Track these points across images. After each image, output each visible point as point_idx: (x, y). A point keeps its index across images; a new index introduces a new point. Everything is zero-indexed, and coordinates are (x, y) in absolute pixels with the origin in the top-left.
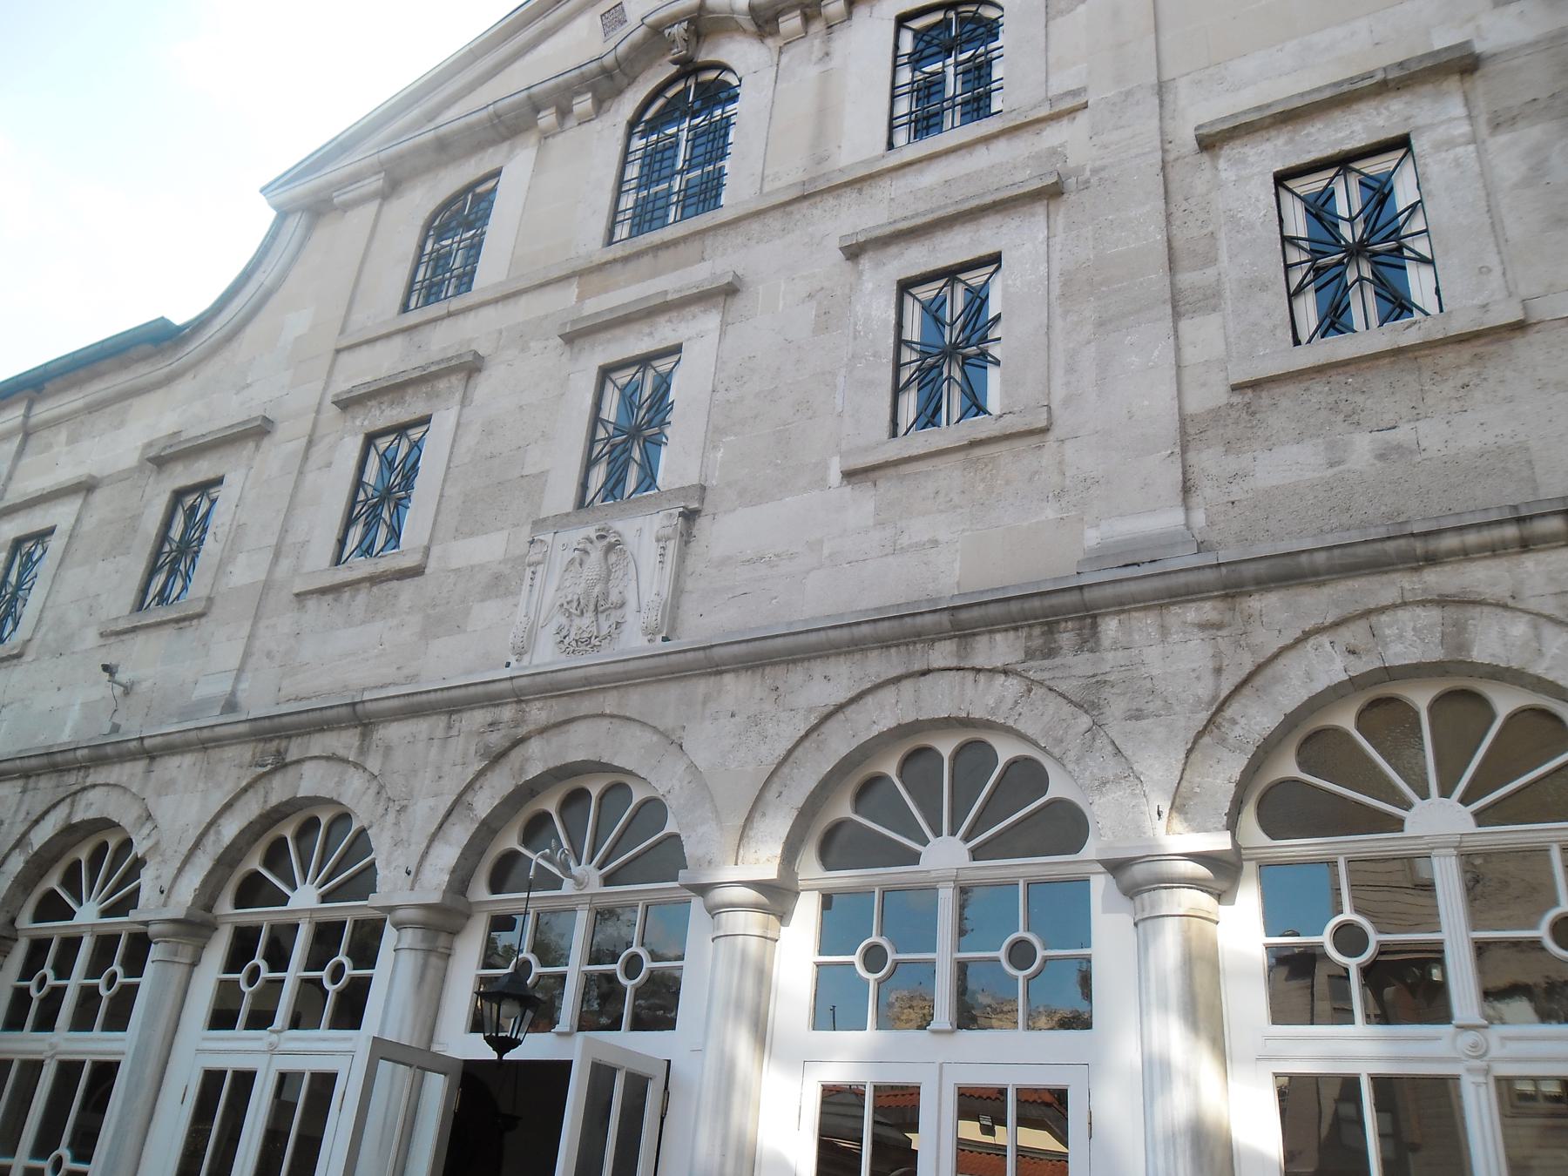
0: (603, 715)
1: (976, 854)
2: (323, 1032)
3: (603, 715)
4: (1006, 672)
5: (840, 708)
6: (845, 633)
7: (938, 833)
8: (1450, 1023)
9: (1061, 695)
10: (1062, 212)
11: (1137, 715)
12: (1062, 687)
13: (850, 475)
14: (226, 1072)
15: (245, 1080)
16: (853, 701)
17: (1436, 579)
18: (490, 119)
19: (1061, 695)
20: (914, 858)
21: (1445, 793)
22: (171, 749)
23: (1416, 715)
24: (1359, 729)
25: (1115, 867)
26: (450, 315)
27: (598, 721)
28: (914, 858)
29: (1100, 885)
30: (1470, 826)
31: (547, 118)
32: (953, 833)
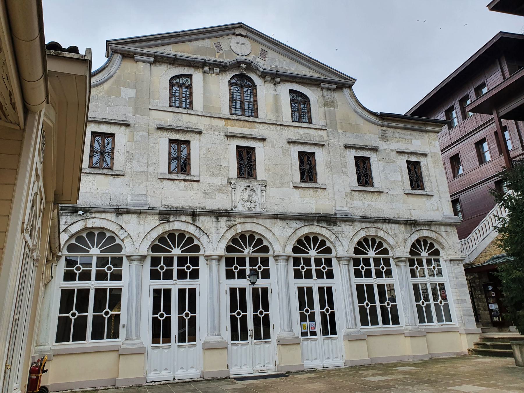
0: (254, 223)
1: (318, 253)
2: (161, 280)
3: (254, 223)
4: (324, 227)
5: (299, 228)
6: (268, 215)
7: (175, 248)
8: (312, 278)
9: (332, 232)
10: (128, 129)
11: (342, 237)
12: (332, 231)
13: (294, 187)
14: (88, 290)
15: (168, 292)
16: (301, 227)
17: (376, 225)
18: (192, 61)
19: (332, 232)
20: (171, 252)
21: (93, 247)
22: (128, 212)
23: (255, 239)
24: (86, 236)
25: (128, 257)
26: (188, 114)
27: (252, 224)
28: (171, 252)
29: (125, 259)
30: (316, 254)
31: (206, 69)
32: (93, 247)
